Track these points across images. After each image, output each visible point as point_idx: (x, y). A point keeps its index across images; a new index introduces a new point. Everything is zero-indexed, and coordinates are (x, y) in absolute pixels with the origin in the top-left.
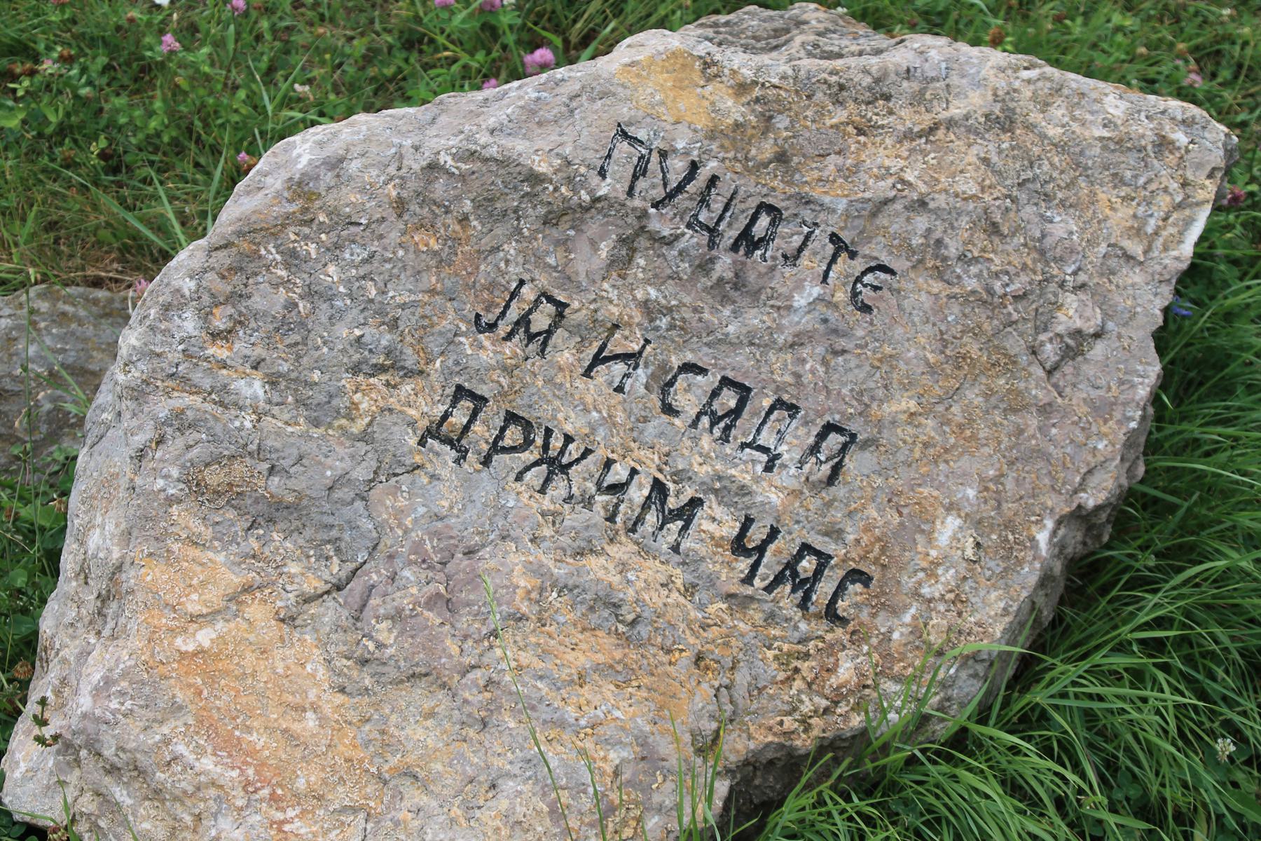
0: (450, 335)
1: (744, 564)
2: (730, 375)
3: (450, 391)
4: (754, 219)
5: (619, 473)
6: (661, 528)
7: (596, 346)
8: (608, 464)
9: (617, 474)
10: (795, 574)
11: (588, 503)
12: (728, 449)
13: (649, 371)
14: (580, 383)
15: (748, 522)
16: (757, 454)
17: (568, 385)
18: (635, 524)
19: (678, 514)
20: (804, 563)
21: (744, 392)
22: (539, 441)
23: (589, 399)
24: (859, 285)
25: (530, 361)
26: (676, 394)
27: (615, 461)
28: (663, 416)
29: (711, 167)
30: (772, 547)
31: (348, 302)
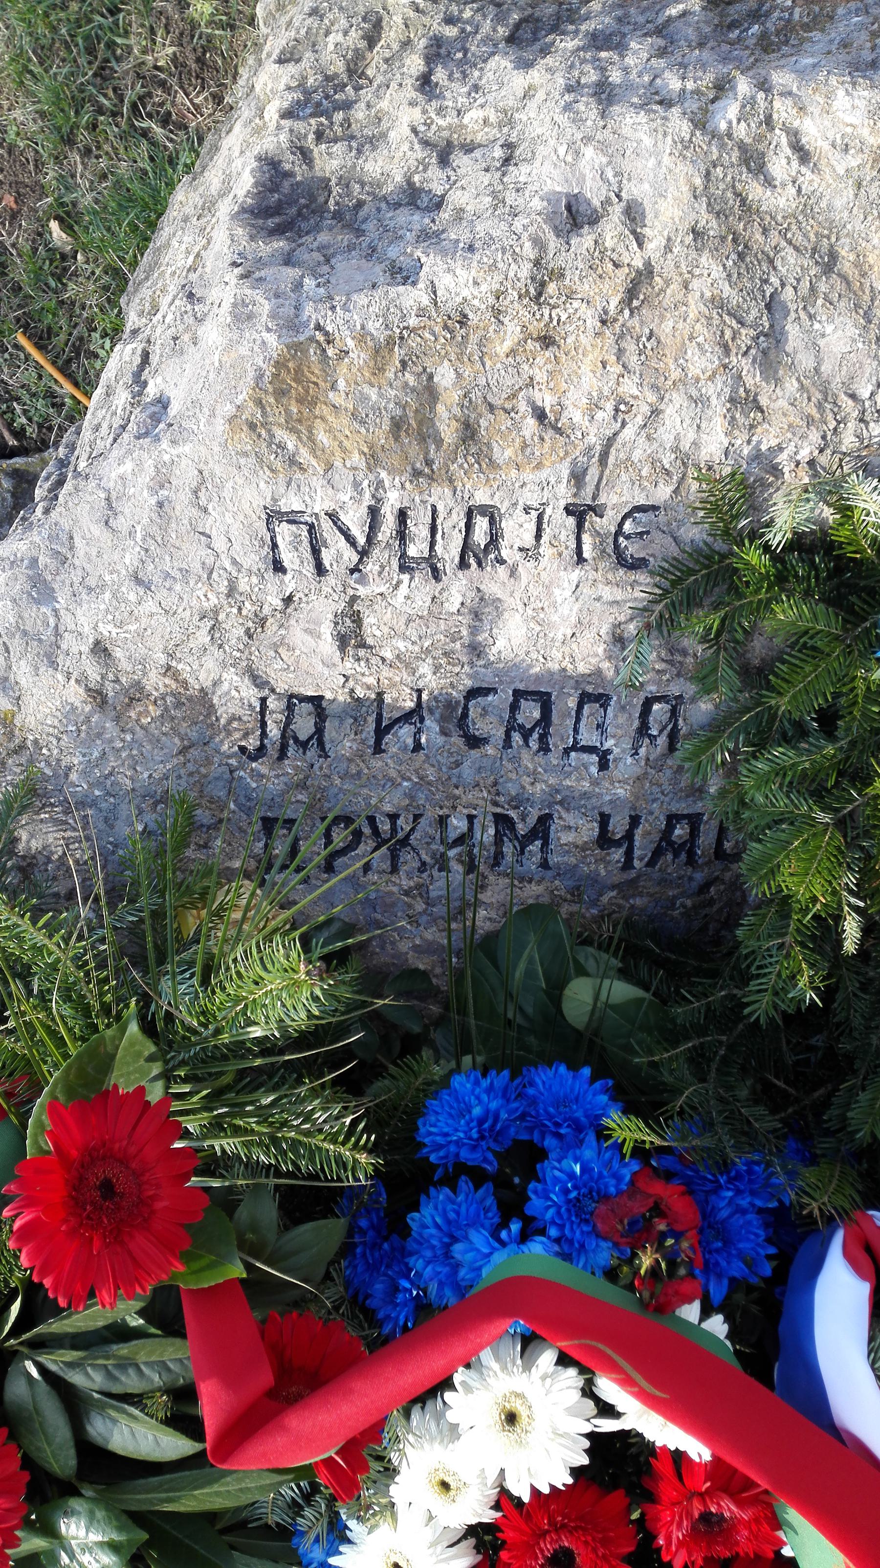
0: (227, 776)
1: (617, 855)
2: (521, 687)
3: (258, 826)
4: (469, 526)
5: (458, 824)
6: (522, 852)
7: (372, 719)
8: (442, 821)
9: (456, 828)
10: (671, 843)
11: (443, 864)
12: (554, 758)
13: (437, 716)
14: (377, 763)
15: (604, 820)
16: (585, 756)
17: (366, 771)
18: (495, 858)
19: (532, 835)
20: (677, 832)
21: (545, 701)
22: (367, 830)
23: (393, 774)
24: (621, 539)
25: (316, 767)
26: (474, 724)
27: (448, 816)
28: (472, 752)
29: (393, 501)
30: (639, 832)
31: (112, 800)
